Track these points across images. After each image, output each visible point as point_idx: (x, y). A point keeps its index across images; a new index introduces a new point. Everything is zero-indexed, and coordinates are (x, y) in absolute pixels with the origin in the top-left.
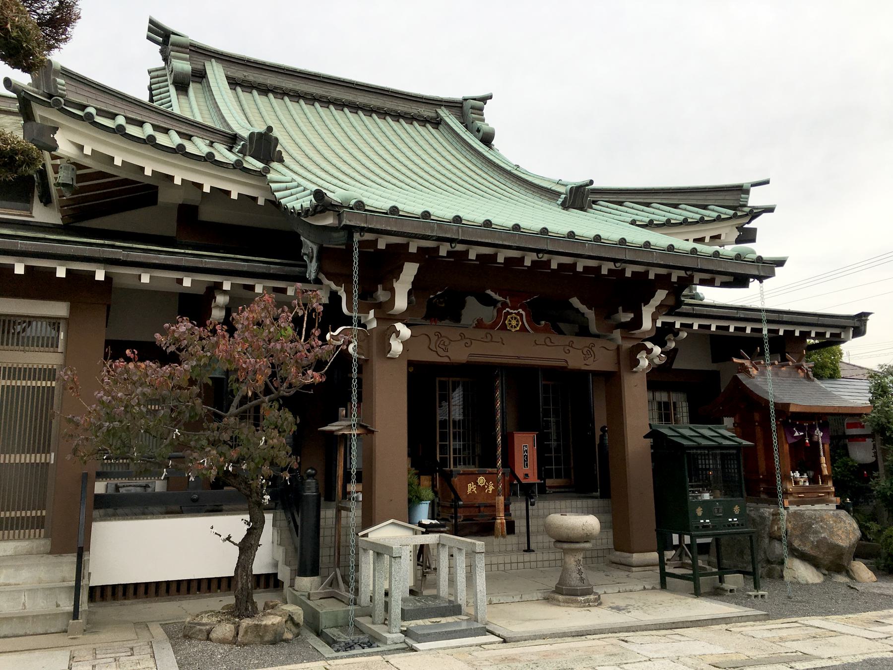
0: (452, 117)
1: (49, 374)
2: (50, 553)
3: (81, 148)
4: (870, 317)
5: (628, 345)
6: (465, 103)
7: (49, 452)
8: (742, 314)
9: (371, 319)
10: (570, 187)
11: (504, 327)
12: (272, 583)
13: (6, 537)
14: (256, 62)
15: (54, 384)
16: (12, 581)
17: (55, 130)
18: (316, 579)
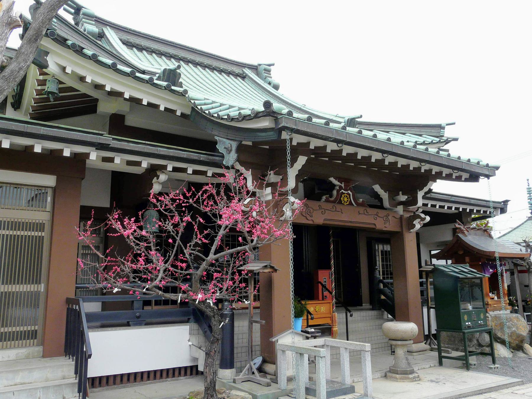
0: (253, 74)
1: (40, 227)
2: (43, 357)
3: (64, 69)
4: (509, 203)
5: (407, 215)
6: (259, 67)
7: (40, 283)
8: (453, 199)
9: (267, 194)
10: (346, 119)
11: (340, 202)
12: (194, 372)
13: (4, 347)
14: (134, 31)
15: (43, 234)
16: (26, 381)
17: (47, 53)
18: (234, 370)
